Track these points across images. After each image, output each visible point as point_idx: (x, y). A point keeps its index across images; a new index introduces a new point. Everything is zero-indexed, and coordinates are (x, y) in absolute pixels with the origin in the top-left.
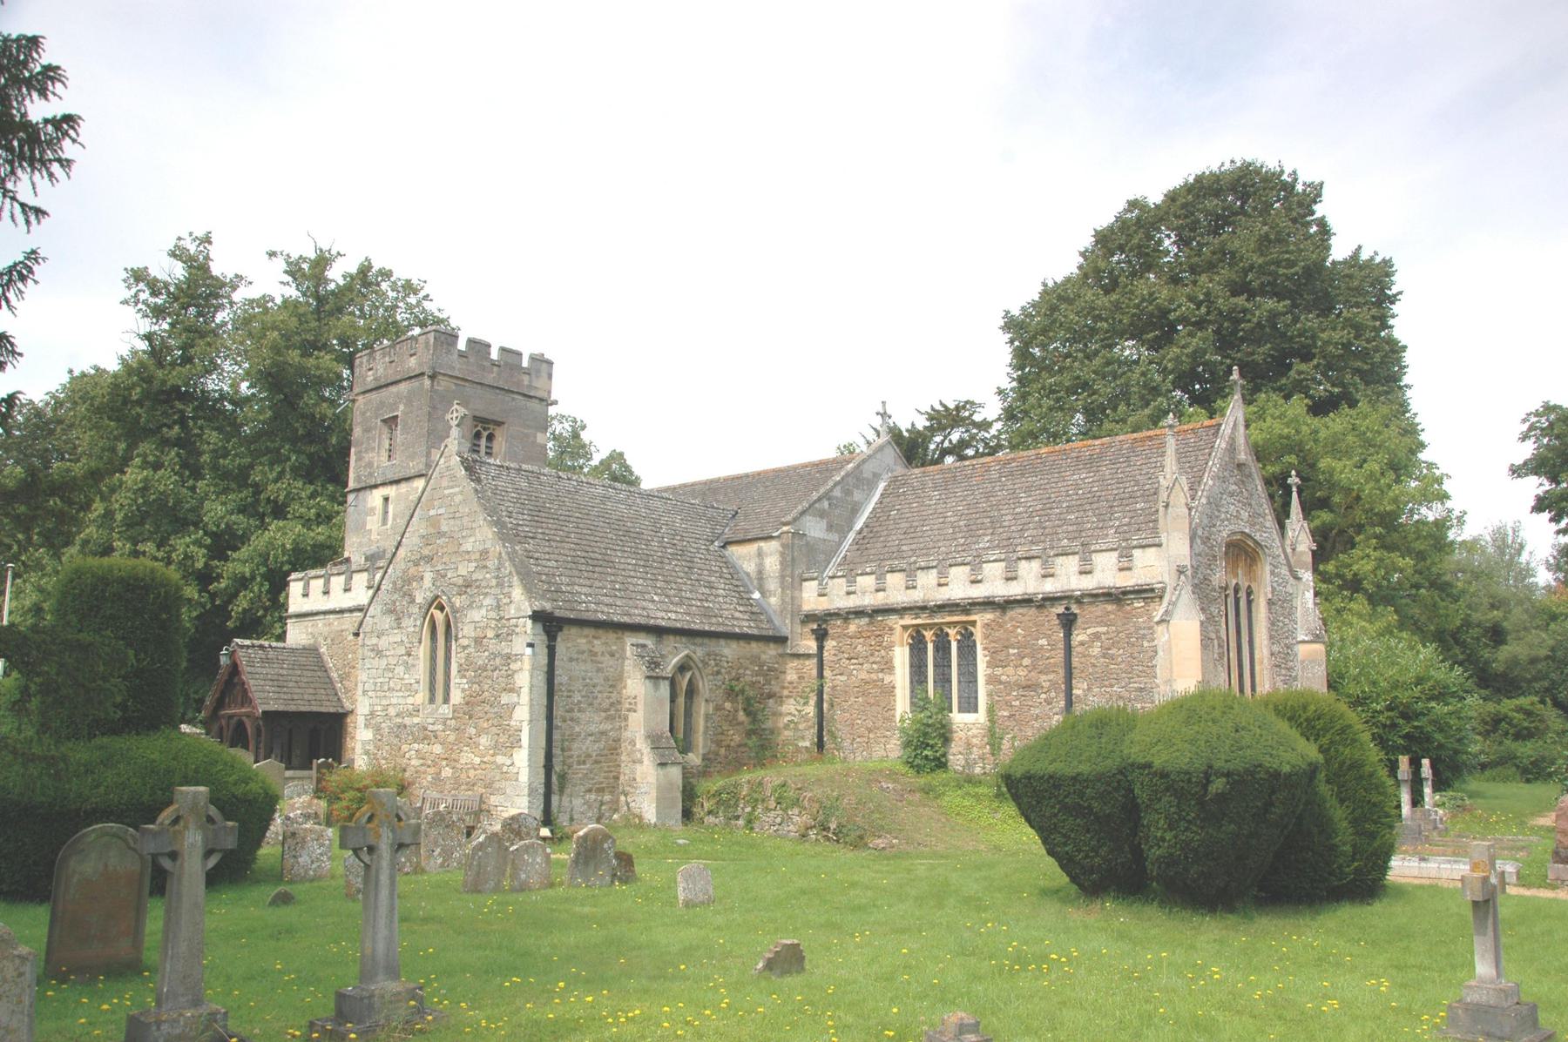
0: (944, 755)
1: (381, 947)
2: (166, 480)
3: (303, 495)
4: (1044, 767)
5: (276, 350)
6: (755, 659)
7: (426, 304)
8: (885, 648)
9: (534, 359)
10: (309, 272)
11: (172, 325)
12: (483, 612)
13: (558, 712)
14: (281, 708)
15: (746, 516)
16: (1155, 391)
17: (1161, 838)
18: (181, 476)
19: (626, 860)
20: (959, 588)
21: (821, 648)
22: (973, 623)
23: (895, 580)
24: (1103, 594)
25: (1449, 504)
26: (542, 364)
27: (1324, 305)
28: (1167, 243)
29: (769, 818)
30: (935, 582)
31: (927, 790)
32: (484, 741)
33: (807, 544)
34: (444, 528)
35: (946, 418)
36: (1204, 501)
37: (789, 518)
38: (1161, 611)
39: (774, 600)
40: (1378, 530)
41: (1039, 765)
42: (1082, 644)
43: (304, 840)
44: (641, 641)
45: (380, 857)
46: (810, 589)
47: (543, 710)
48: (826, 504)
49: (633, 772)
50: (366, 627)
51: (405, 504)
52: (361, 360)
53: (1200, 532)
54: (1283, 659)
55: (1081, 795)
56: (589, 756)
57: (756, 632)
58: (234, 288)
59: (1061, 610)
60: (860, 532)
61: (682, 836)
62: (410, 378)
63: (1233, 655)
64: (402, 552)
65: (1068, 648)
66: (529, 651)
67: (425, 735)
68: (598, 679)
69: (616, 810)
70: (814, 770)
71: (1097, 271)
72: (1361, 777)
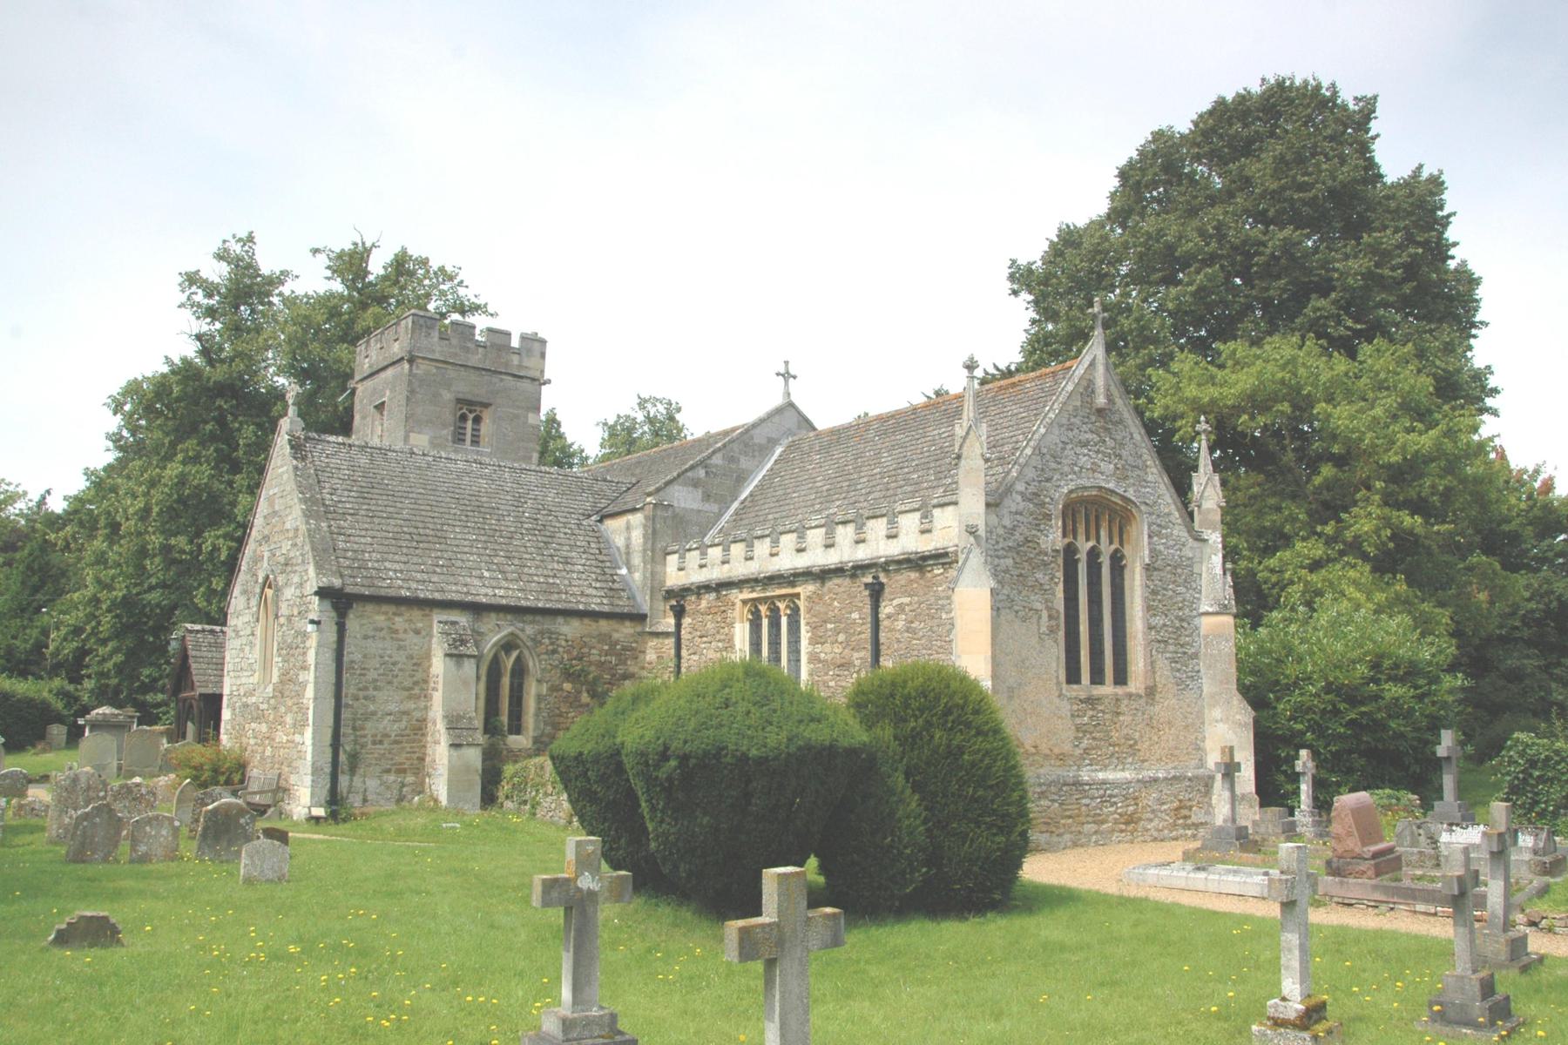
2: (202, 474)
7: (462, 291)
10: (351, 264)
13: (349, 690)
20: (788, 561)
21: (678, 625)
22: (798, 595)
26: (535, 345)
33: (675, 516)
37: (652, 489)
42: (889, 617)
44: (453, 618)
47: (331, 689)
48: (701, 473)
56: (388, 736)
57: (606, 609)
59: (869, 579)
62: (394, 363)
68: (400, 657)
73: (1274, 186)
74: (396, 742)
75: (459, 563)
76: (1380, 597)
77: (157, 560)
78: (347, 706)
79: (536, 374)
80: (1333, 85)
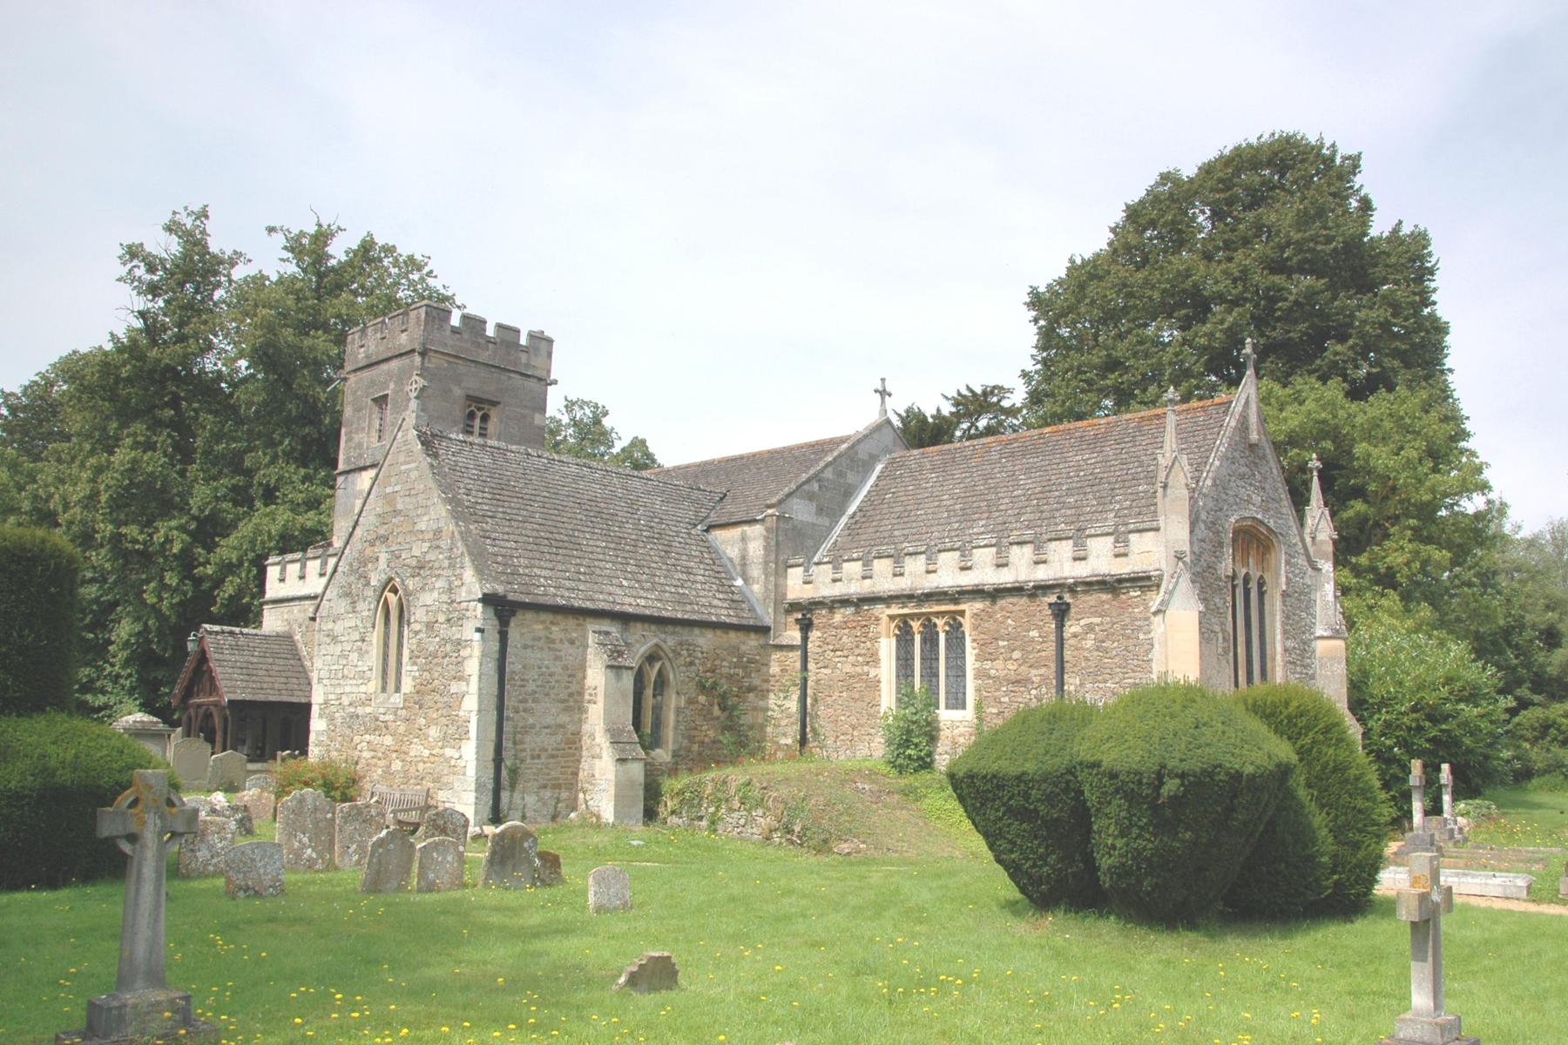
0: (930, 754)
1: (141, 950)
2: (154, 462)
3: (295, 478)
5: (270, 328)
6: (734, 650)
7: (431, 281)
8: (871, 640)
9: (532, 336)
10: (310, 248)
11: (167, 302)
12: (435, 595)
13: (510, 702)
14: (249, 697)
15: (734, 499)
16: (1187, 374)
17: (1112, 847)
18: (172, 458)
19: (551, 861)
20: (948, 575)
21: (805, 639)
22: (962, 613)
23: (882, 567)
24: (1098, 582)
25: (1491, 496)
26: (542, 343)
27: (1365, 285)
28: (1201, 219)
29: (732, 820)
30: (923, 568)
31: (906, 792)
32: (434, 732)
33: (794, 528)
34: (400, 507)
35: (975, 403)
36: (1209, 482)
37: (774, 500)
38: (1159, 600)
40: (1412, 522)
41: (983, 763)
43: (203, 834)
44: (604, 628)
45: (144, 846)
46: (795, 576)
47: (493, 701)
48: (816, 486)
49: (592, 767)
50: (323, 611)
51: (390, 481)
52: (354, 336)
53: (1203, 516)
54: (1301, 655)
55: (1027, 796)
57: (735, 621)
58: (233, 264)
59: (1053, 599)
60: (853, 516)
61: (639, 835)
62: (401, 355)
63: (1241, 650)
66: (477, 636)
67: (377, 726)
69: (574, 809)
70: (793, 768)
71: (1128, 248)
72: (1347, 781)
73: (1296, 236)
74: (553, 756)
75: (598, 571)
76: (1409, 623)
77: (103, 551)
78: (509, 718)
79: (542, 374)
80: (1333, 145)
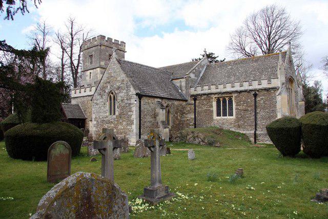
4: (275, 126)
6: (181, 105)
20: (229, 88)
21: (195, 102)
30: (223, 87)
32: (124, 123)
39: (184, 92)
59: (254, 93)
60: (202, 77)
64: (102, 81)
65: (255, 101)
